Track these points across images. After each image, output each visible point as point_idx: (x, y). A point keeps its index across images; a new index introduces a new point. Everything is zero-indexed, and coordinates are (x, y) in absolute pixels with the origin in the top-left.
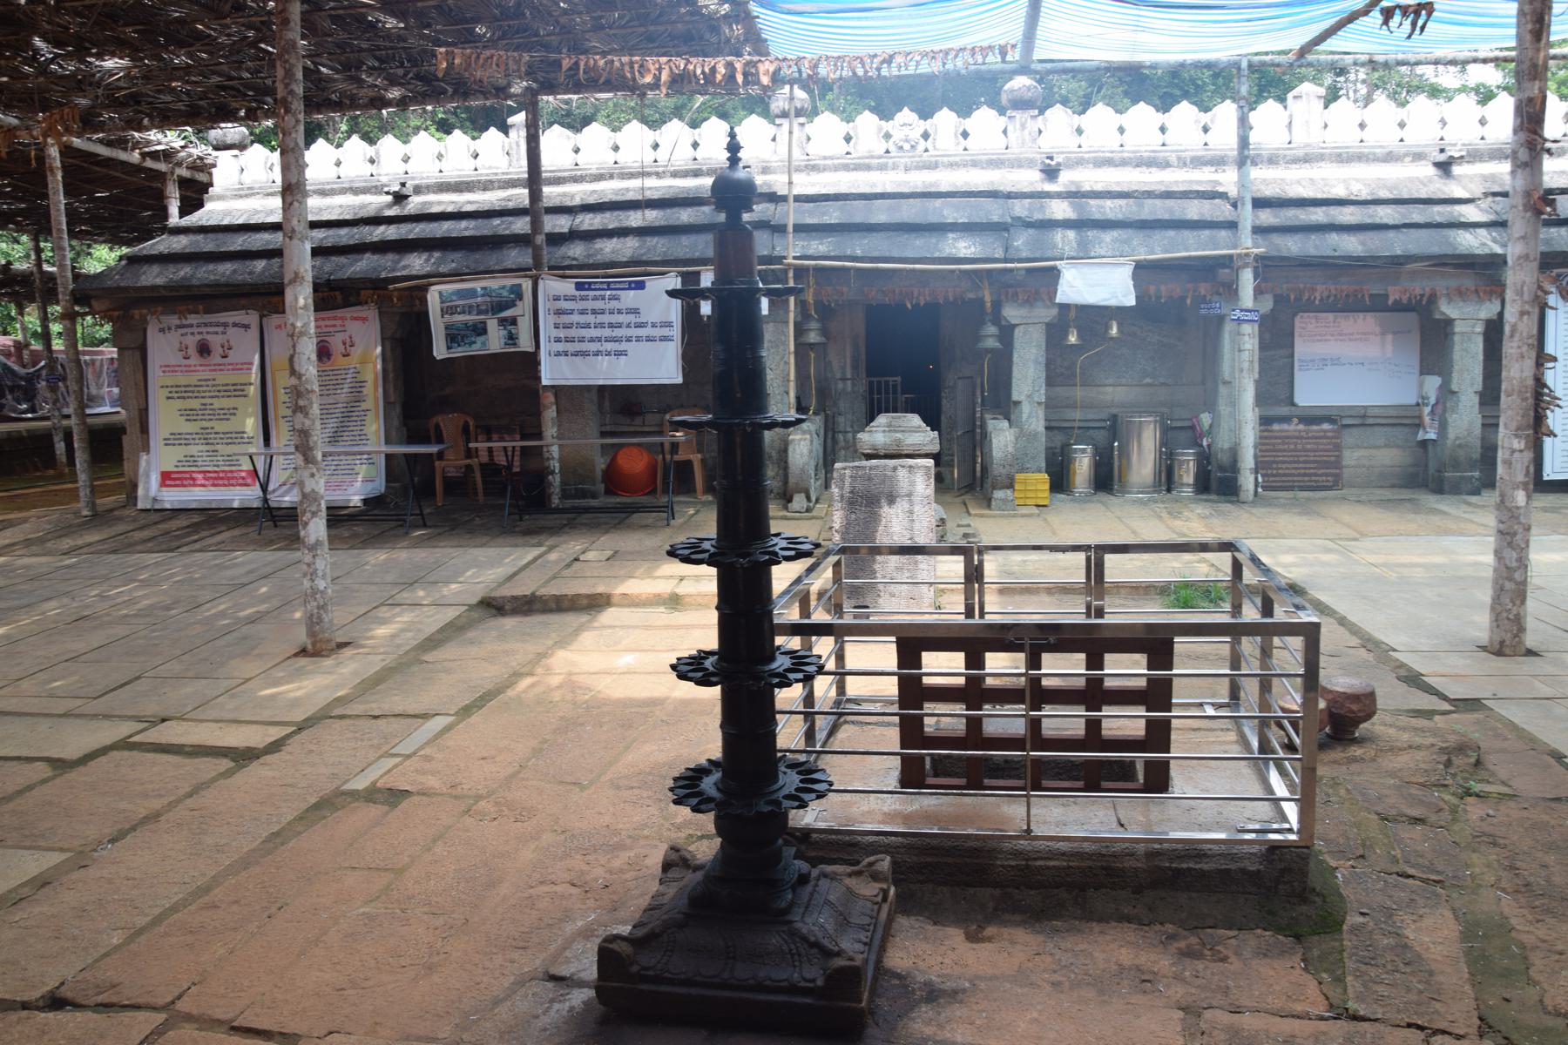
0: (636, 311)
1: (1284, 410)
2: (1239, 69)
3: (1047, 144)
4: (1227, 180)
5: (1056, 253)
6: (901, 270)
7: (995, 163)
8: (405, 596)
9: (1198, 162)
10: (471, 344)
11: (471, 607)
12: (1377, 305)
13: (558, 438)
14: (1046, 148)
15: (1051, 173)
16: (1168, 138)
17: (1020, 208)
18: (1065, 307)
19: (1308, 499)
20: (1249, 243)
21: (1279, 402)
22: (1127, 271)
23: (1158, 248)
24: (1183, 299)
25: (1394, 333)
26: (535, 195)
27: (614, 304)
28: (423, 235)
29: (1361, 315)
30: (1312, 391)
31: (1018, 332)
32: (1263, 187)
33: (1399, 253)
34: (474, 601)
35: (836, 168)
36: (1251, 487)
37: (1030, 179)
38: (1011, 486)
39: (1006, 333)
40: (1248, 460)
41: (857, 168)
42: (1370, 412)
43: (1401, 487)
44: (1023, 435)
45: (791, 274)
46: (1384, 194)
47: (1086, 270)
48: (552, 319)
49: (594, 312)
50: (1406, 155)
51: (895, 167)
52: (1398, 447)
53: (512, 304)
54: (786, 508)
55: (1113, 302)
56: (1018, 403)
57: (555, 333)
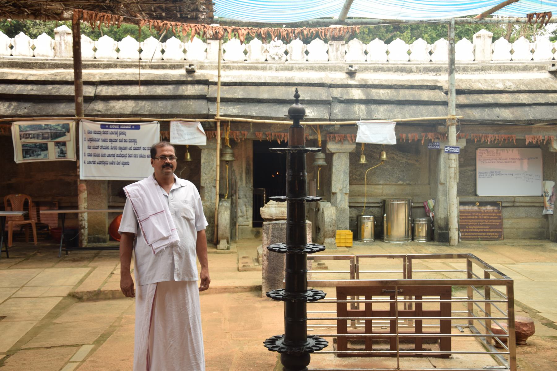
0: (134, 141)
1: (472, 198)
2: (450, 24)
3: (349, 59)
4: (443, 79)
5: (356, 117)
6: (277, 124)
7: (322, 68)
8: (21, 293)
9: (427, 70)
10: (38, 155)
11: (65, 298)
12: (520, 144)
13: (88, 208)
14: (349, 61)
15: (351, 74)
16: (412, 57)
17: (336, 93)
18: (359, 144)
19: (486, 244)
20: (454, 113)
21: (468, 194)
22: (393, 126)
23: (409, 115)
24: (419, 141)
25: (529, 159)
26: (78, 74)
27: (122, 137)
28: (4, 92)
29: (511, 149)
30: (486, 188)
31: (335, 157)
32: (460, 84)
33: (531, 118)
34: (65, 294)
35: (239, 68)
36: (457, 238)
37: (340, 77)
38: (334, 236)
39: (329, 157)
40: (454, 224)
41: (250, 68)
42: (517, 200)
43: (534, 239)
44: (340, 211)
45: (219, 124)
46: (523, 88)
47: (371, 126)
48: (87, 144)
49: (111, 141)
50: (535, 67)
51: (270, 69)
52: (532, 218)
53: (63, 134)
54: (217, 248)
55: (385, 142)
56: (334, 194)
57: (88, 151)
